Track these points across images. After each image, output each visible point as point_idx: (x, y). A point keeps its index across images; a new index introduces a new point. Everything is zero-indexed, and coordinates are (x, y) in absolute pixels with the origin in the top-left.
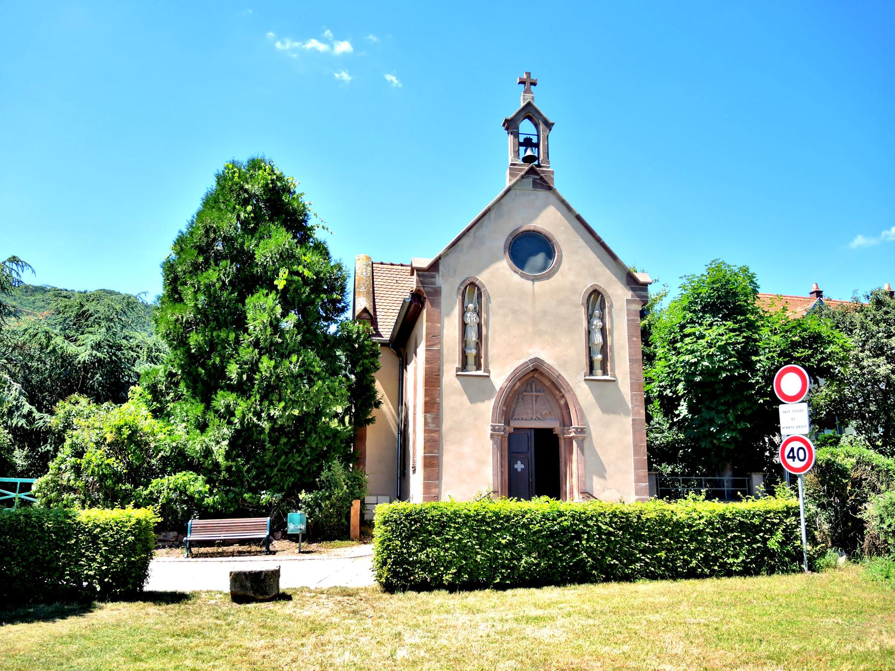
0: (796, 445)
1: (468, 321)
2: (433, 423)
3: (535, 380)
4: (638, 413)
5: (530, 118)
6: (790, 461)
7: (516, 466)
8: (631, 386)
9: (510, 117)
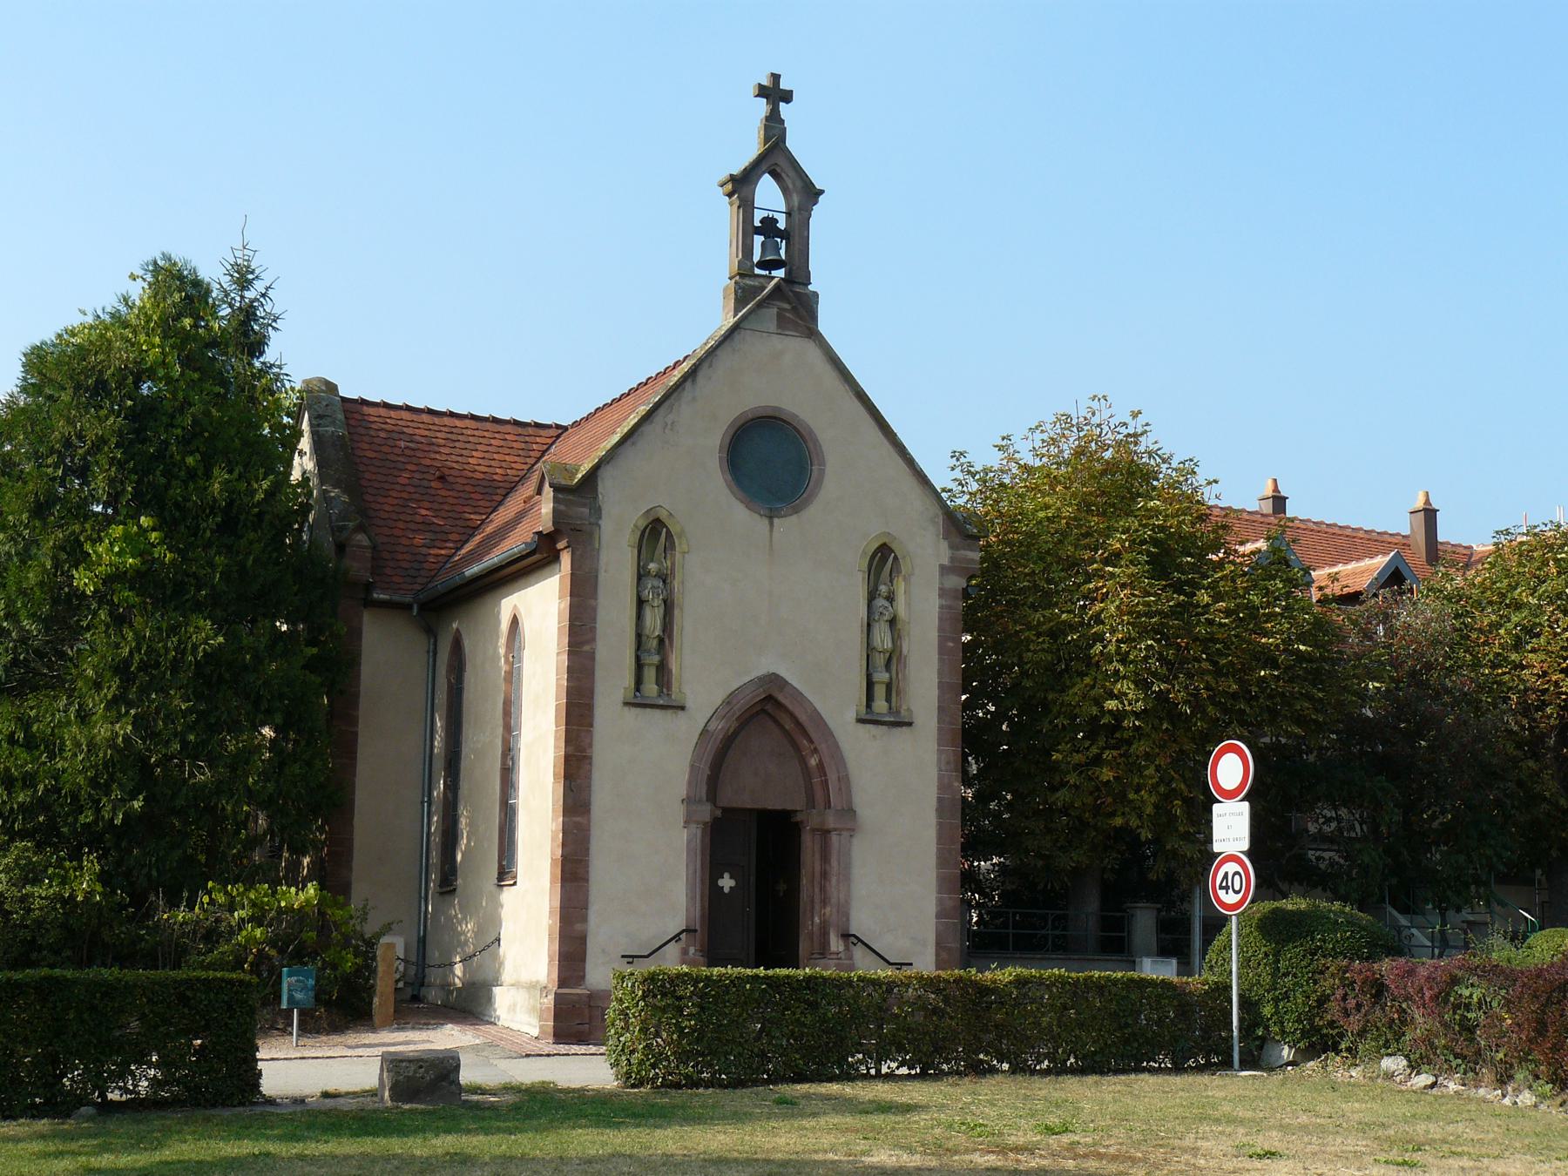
0: (1231, 867)
1: (648, 594)
3: (767, 713)
5: (775, 175)
6: (1221, 893)
7: (721, 883)
9: (737, 168)
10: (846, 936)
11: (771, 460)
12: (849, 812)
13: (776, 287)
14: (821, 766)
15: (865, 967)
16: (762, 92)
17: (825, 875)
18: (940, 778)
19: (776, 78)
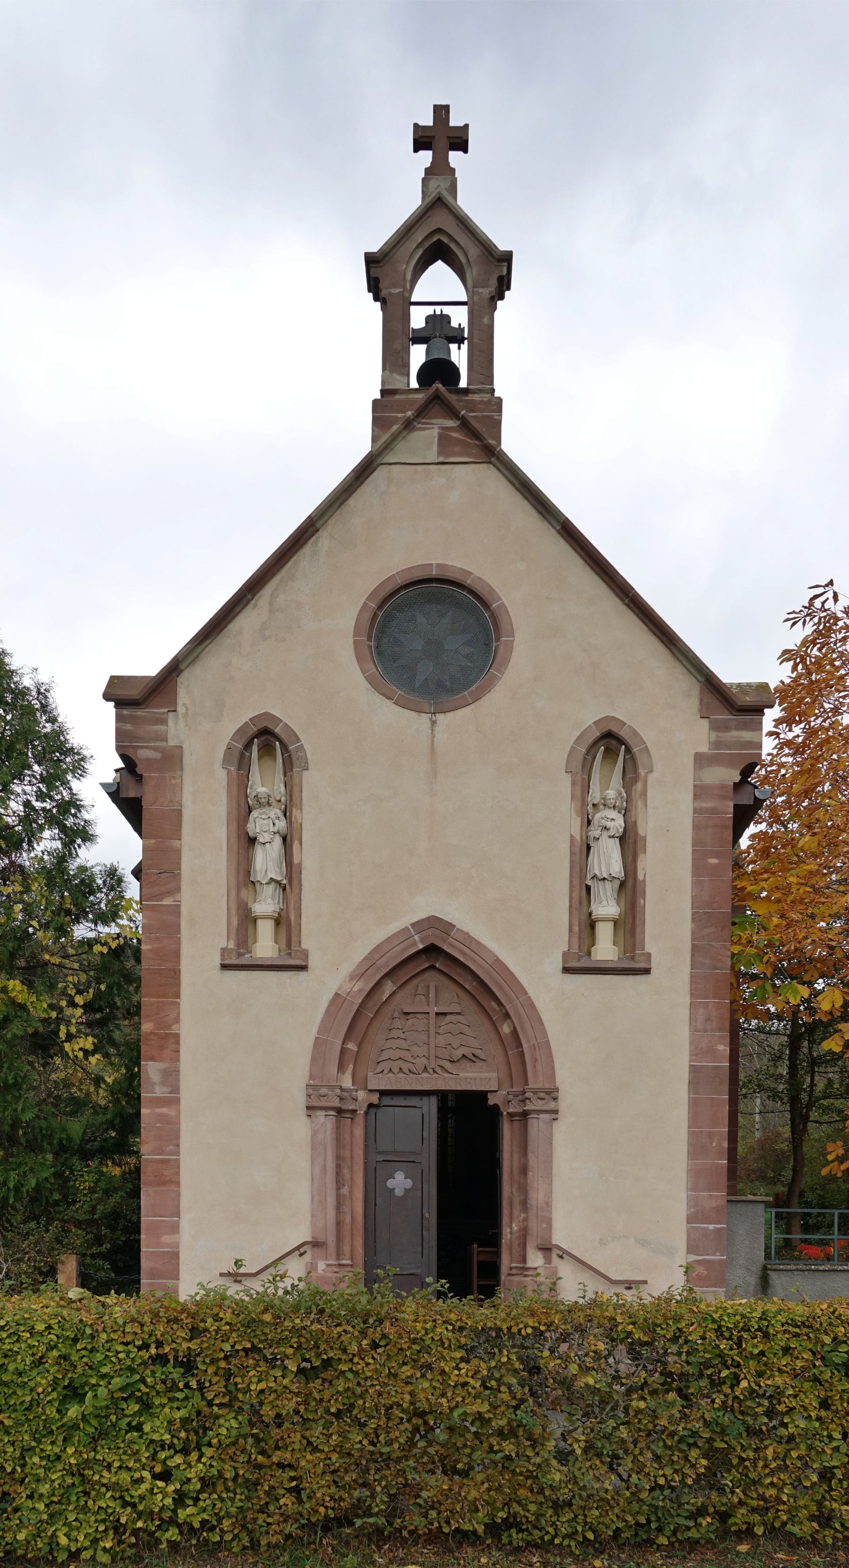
2: (163, 1083)
4: (711, 1051)
8: (692, 982)
10: (546, 1249)
11: (433, 636)
12: (552, 1093)
13: (440, 402)
14: (515, 1032)
15: (572, 1288)
16: (422, 140)
17: (524, 1170)
18: (694, 1043)
19: (441, 112)
